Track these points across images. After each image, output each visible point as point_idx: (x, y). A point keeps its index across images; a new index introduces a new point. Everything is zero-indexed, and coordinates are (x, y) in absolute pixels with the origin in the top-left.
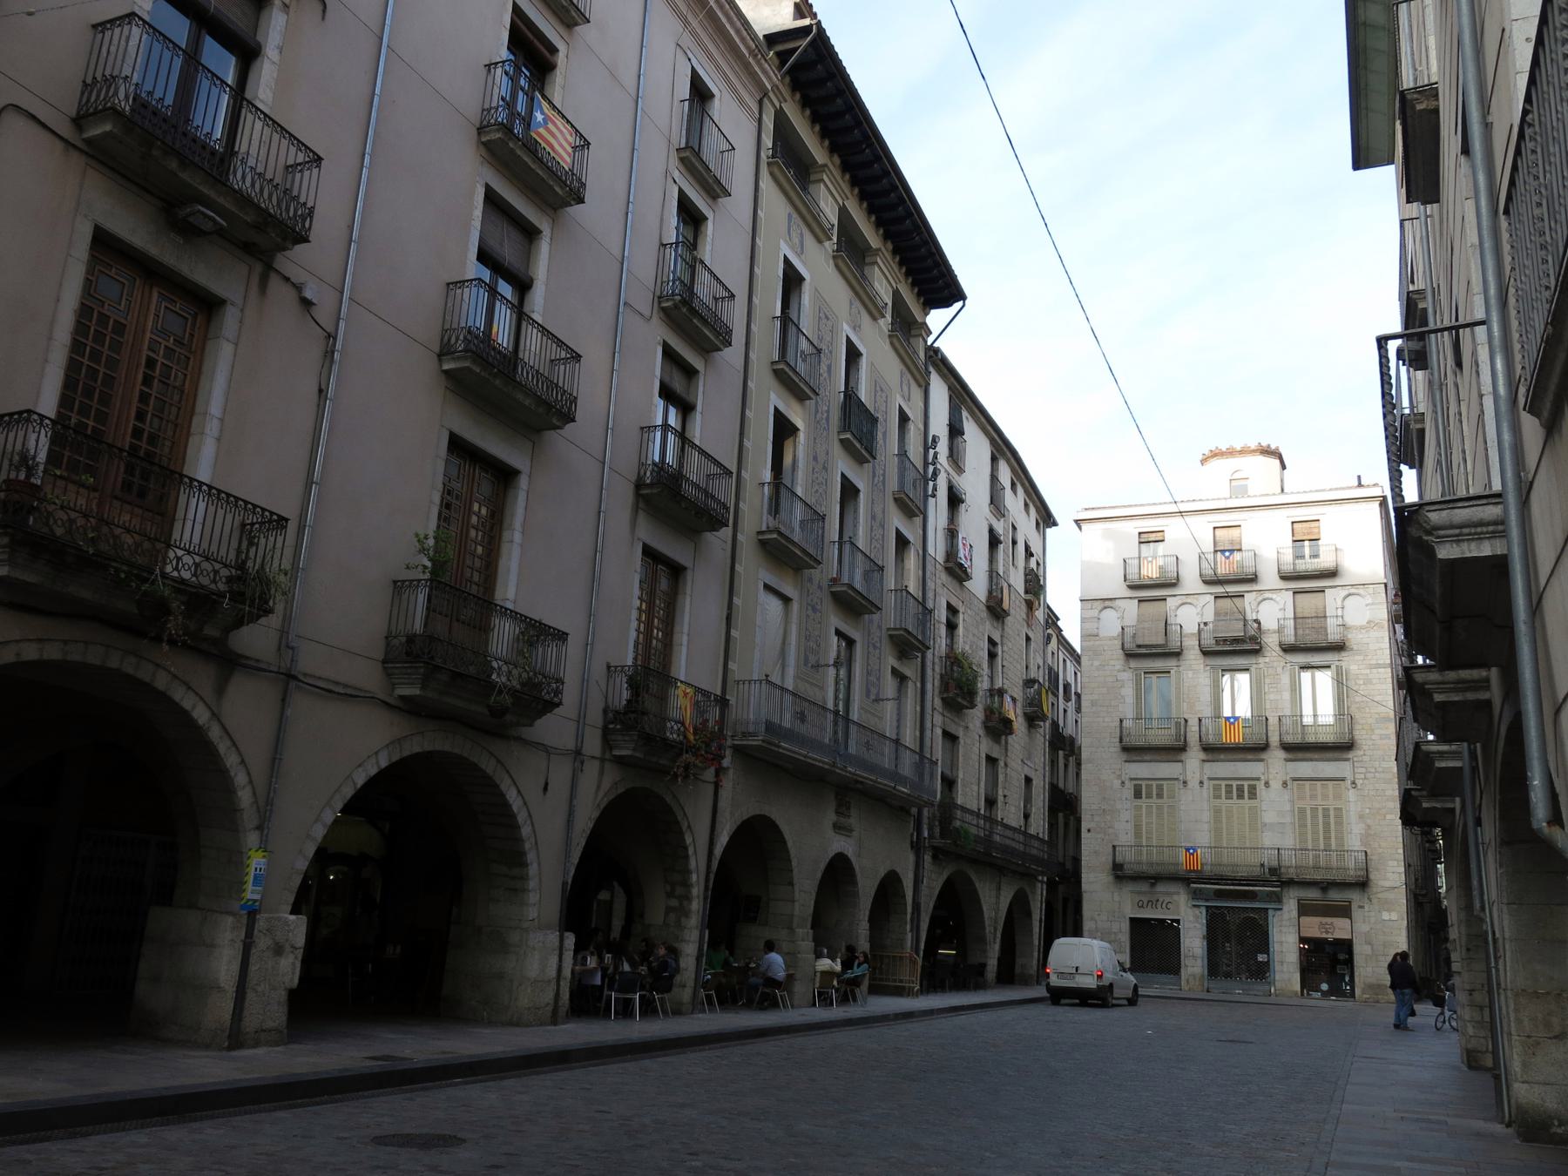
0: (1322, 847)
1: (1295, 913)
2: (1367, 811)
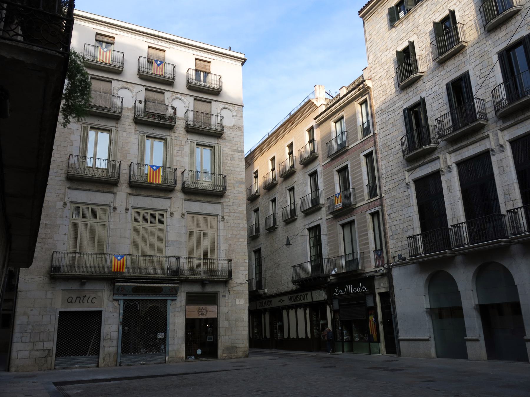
0: (202, 257)
1: (184, 302)
2: (230, 236)
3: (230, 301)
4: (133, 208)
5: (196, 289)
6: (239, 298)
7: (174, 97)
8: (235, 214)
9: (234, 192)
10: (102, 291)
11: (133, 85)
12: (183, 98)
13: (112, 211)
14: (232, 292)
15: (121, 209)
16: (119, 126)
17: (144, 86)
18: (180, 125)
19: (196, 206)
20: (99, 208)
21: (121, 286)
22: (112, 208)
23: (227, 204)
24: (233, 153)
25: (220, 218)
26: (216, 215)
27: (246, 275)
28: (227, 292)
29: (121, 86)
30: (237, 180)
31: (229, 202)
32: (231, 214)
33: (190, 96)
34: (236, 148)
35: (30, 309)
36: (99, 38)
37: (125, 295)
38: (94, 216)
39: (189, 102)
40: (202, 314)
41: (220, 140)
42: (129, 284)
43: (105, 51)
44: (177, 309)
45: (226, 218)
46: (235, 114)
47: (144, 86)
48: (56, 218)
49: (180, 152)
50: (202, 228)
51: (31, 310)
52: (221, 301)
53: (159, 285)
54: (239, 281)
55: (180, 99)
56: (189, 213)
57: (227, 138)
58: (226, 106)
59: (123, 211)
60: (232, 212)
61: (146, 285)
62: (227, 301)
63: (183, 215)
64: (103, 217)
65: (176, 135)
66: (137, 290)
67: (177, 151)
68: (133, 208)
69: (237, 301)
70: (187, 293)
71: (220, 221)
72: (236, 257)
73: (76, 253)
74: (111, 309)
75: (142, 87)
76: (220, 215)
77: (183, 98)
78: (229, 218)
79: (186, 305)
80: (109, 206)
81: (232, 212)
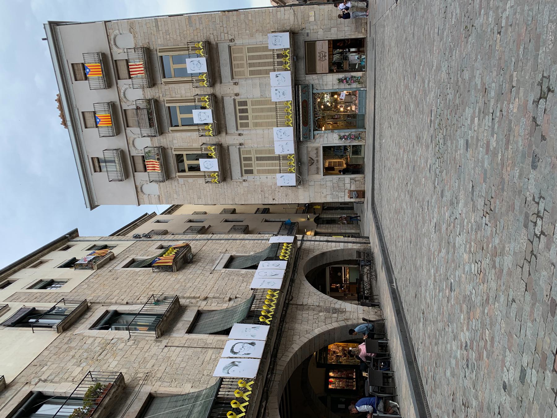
1: (314, 76)
2: (247, 31)
3: (311, 28)
4: (237, 129)
5: (302, 65)
6: (309, 17)
7: (124, 100)
8: (225, 26)
9: (201, 28)
10: (307, 147)
11: (128, 139)
12: (122, 91)
13: (243, 146)
14: (303, 26)
15: (241, 140)
16: (169, 147)
17: (125, 129)
18: (151, 93)
19: (225, 71)
20: (242, 156)
21: (303, 136)
22: (240, 146)
23: (216, 36)
24: (161, 32)
25: (231, 44)
26: (230, 47)
27: (285, 10)
28: (303, 31)
29: (133, 148)
30: (188, 26)
31: (213, 34)
32: (225, 32)
33: (117, 84)
34: (155, 28)
35: (322, 195)
36: (98, 169)
37: (310, 131)
38: (249, 159)
39: (124, 84)
40: (325, 56)
41: (152, 48)
42: (301, 130)
43: (90, 70)
44: (320, 83)
45: (230, 38)
46: (117, 32)
47: (125, 129)
48: (255, 185)
49: (176, 90)
50: (245, 62)
51: (323, 193)
52: (312, 37)
53: (301, 104)
54: (292, 18)
55: (124, 93)
56: (233, 78)
57: (147, 41)
58: (112, 42)
59: (242, 137)
60: (223, 30)
61: (301, 116)
62: (312, 31)
63: (235, 84)
64: (249, 152)
65: (161, 95)
66: (306, 123)
67: (177, 93)
68: (237, 129)
69: (312, 19)
70: (306, 74)
71: (234, 43)
72: (268, 23)
73: (280, 169)
74: (322, 140)
75: (127, 131)
76: (228, 44)
77: (122, 91)
78: (229, 33)
79: (317, 74)
80: (239, 149)
81: (223, 30)
